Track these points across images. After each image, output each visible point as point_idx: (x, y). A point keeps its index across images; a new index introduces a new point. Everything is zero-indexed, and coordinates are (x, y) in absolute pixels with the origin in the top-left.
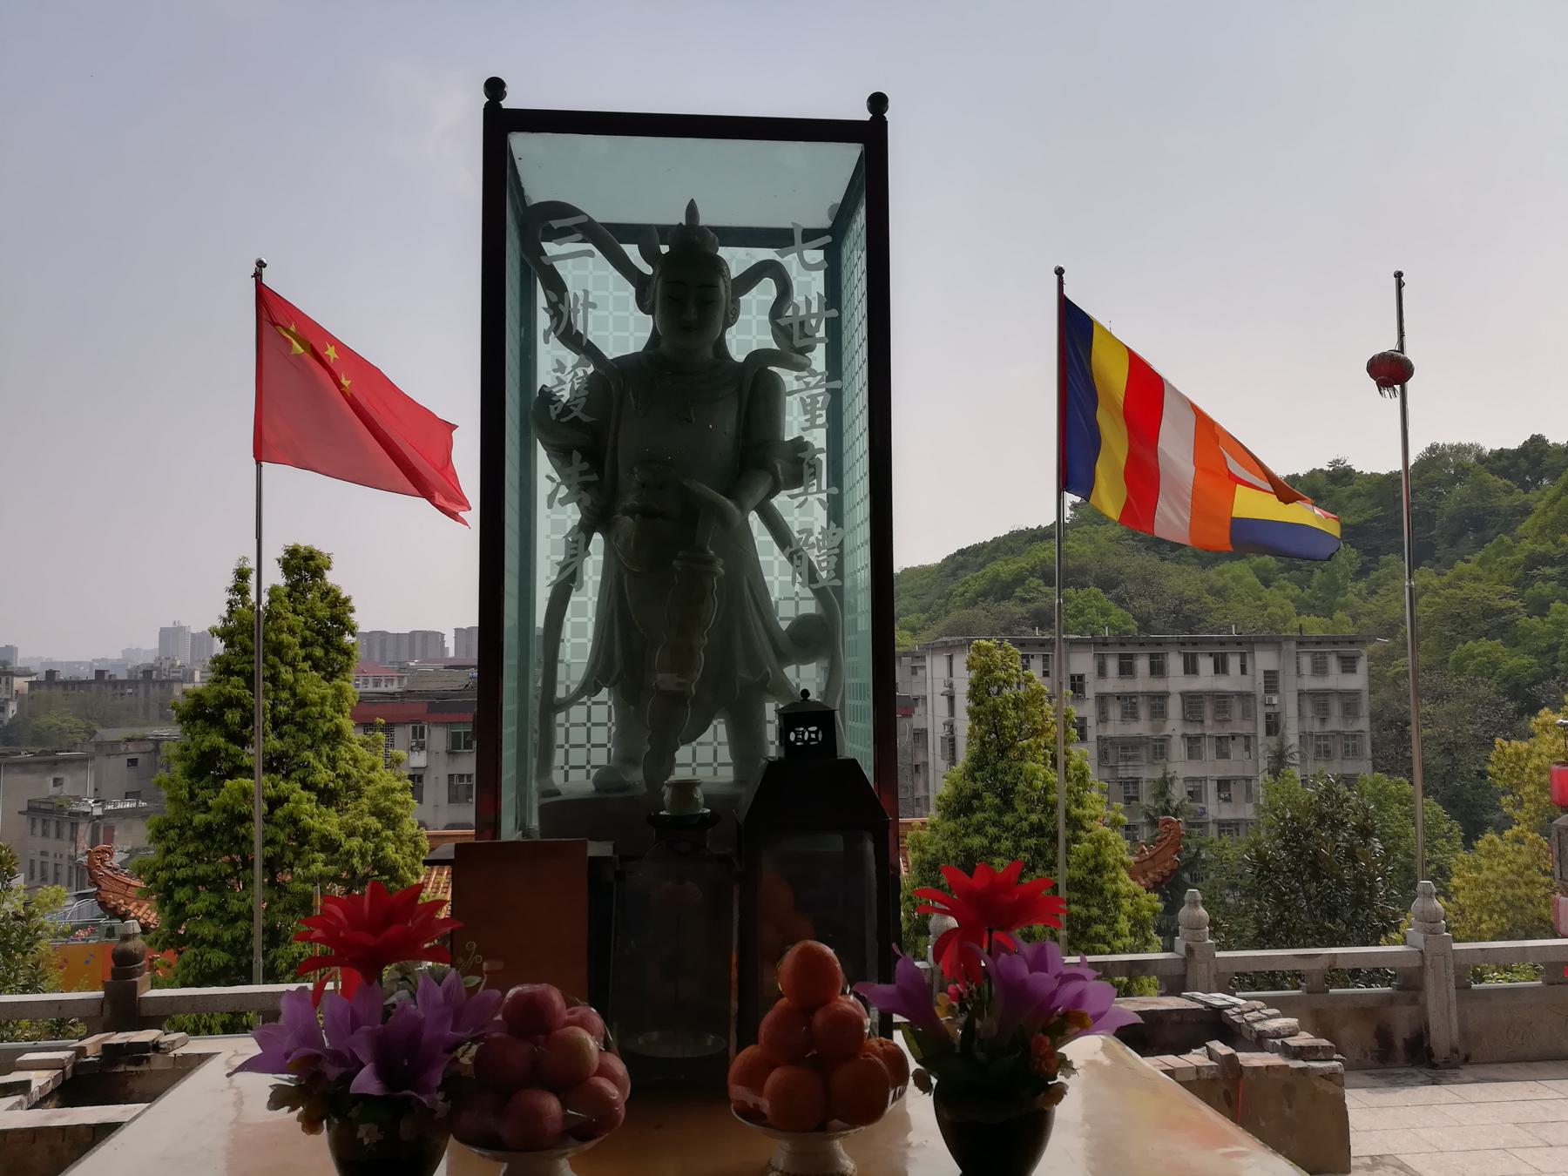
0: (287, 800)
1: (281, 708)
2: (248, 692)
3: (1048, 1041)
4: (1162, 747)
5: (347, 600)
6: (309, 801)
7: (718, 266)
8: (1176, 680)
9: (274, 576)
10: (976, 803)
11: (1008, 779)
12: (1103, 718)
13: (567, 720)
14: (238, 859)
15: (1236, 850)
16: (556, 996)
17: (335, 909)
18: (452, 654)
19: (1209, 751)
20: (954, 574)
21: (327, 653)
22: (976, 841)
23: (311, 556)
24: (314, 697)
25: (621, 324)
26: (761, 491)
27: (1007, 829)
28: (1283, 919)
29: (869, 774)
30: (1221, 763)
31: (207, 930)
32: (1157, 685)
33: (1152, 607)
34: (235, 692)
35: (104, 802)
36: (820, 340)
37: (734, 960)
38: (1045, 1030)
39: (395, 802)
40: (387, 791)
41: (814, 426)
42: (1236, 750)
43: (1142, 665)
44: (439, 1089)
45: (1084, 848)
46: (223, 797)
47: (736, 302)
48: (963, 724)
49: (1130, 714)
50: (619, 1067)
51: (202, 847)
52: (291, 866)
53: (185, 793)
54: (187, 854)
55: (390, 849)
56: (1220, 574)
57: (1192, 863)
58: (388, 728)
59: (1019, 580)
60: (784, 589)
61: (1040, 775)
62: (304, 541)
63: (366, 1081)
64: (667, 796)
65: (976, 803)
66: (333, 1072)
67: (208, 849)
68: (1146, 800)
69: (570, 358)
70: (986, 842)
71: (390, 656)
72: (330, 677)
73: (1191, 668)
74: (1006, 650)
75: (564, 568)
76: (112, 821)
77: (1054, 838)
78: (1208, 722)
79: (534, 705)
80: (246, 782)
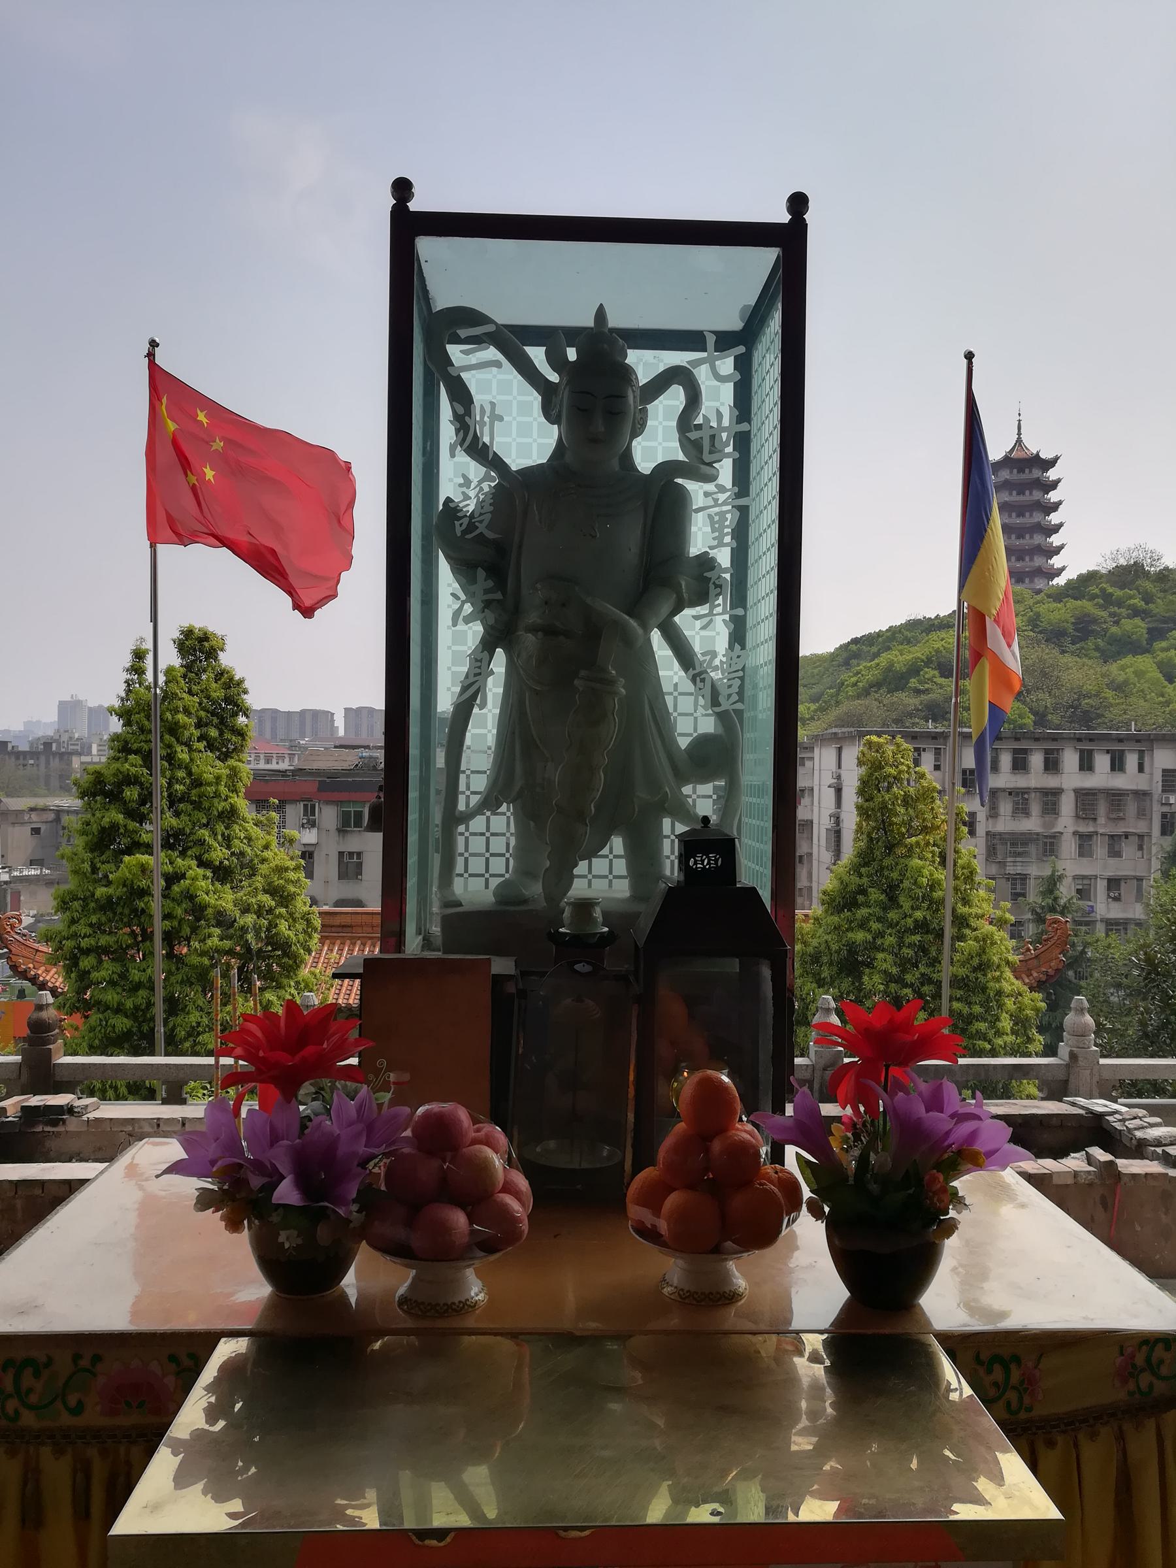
0: (183, 876)
1: (177, 787)
2: (145, 771)
3: (941, 1177)
4: (1052, 844)
5: (241, 682)
6: (205, 877)
7: (626, 374)
8: (1071, 777)
9: (170, 657)
10: (861, 898)
11: (895, 875)
12: (993, 814)
13: (467, 830)
14: (137, 930)
15: (1121, 950)
16: (463, 1114)
17: (253, 1027)
18: (341, 733)
19: (1100, 849)
20: (847, 663)
21: (221, 734)
22: (860, 936)
23: (205, 637)
24: (208, 777)
25: (526, 435)
26: (665, 610)
27: (891, 925)
28: (1169, 1022)
29: (766, 895)
30: (1112, 861)
31: (111, 997)
32: (1051, 782)
33: (1049, 702)
34: (133, 770)
35: (11, 869)
36: (728, 455)
37: (631, 1078)
38: (939, 1166)
39: (288, 881)
40: (280, 870)
41: (722, 544)
42: (1129, 849)
43: (1036, 760)
44: (354, 1201)
45: (969, 945)
46: (123, 872)
47: (644, 411)
48: (850, 820)
49: (1021, 809)
50: (522, 1183)
51: (104, 919)
52: (188, 939)
53: (87, 866)
54: (91, 925)
55: (283, 926)
56: (1123, 668)
57: (1077, 961)
58: (280, 808)
59: (914, 670)
60: (691, 720)
61: (926, 872)
62: (199, 623)
63: (286, 1192)
64: (567, 914)
65: (861, 898)
66: (256, 1182)
67: (110, 921)
68: (1033, 896)
69: (475, 470)
70: (869, 937)
71: (281, 734)
72: (224, 757)
73: (1086, 765)
74: (898, 746)
75: (464, 689)
76: (19, 886)
77: (940, 935)
78: (1102, 820)
79: (437, 816)
80: (144, 858)
